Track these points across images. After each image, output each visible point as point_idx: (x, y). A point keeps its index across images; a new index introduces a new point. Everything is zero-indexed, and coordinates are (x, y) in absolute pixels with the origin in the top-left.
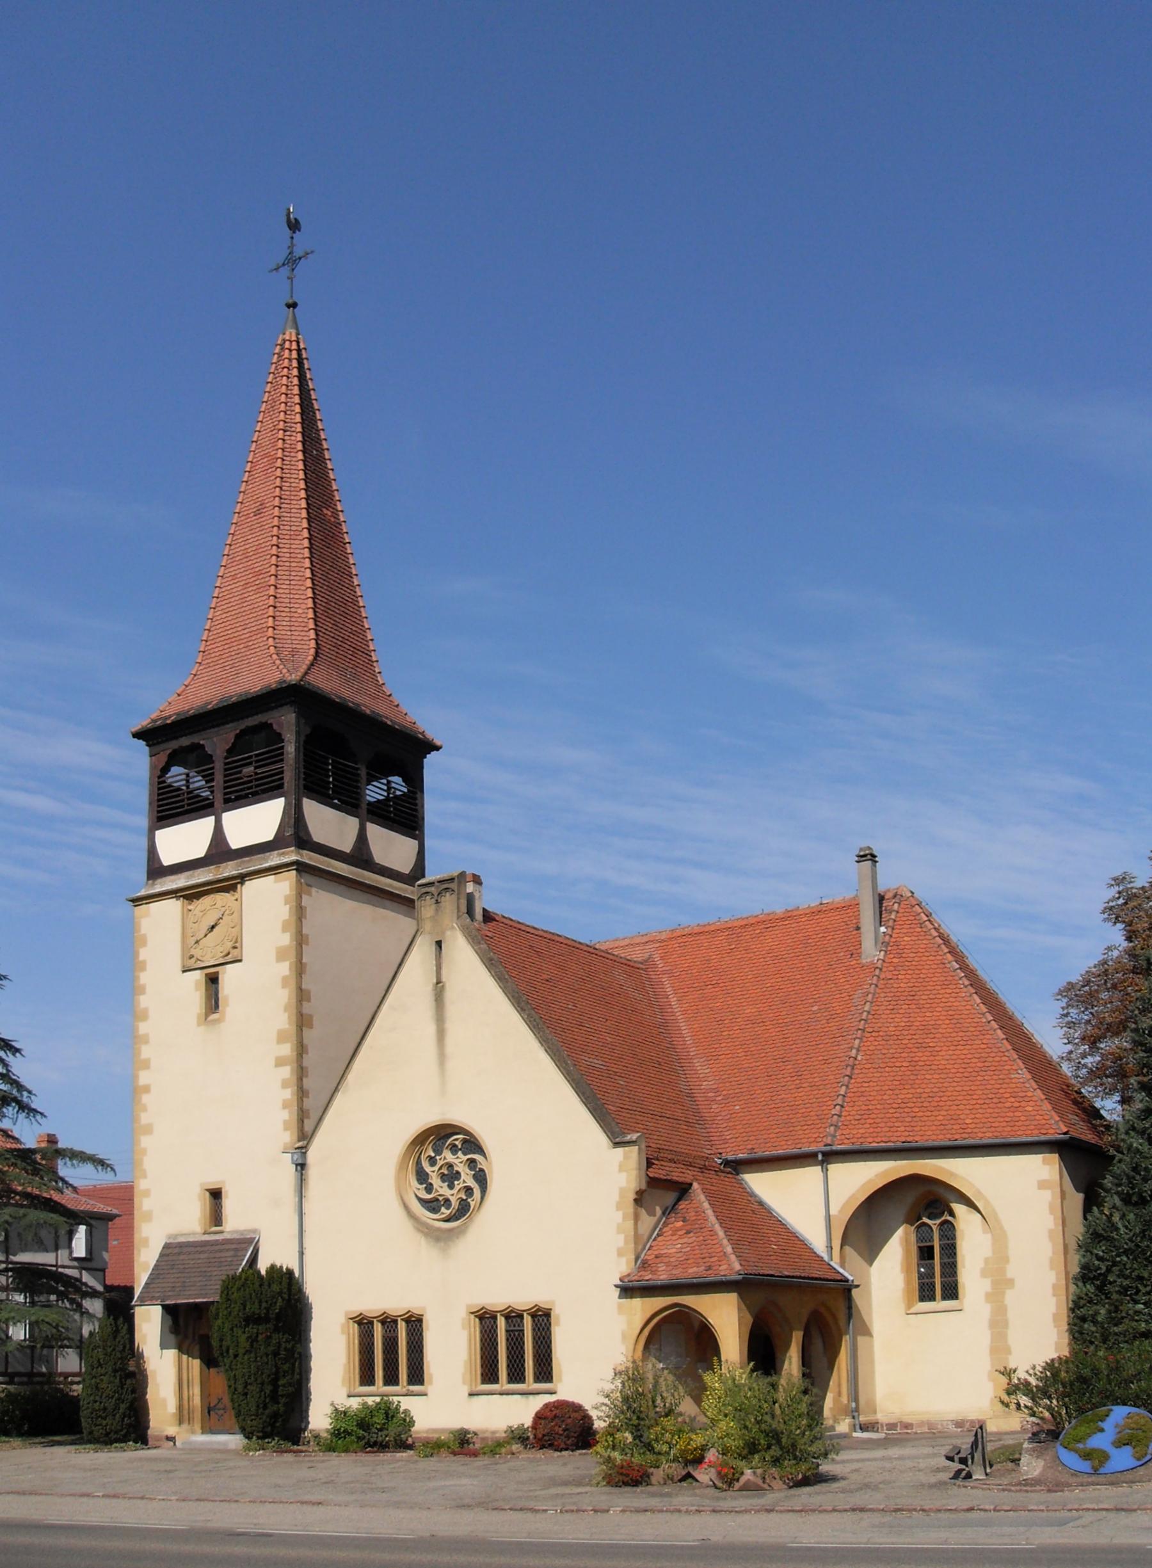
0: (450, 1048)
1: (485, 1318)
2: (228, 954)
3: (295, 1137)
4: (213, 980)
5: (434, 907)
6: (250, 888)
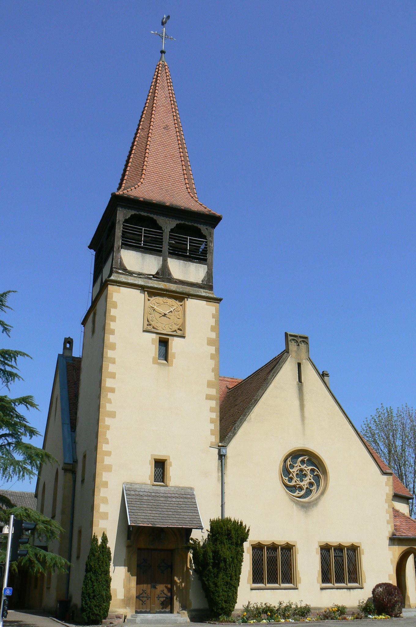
0: (306, 414)
1: (325, 549)
2: (175, 331)
3: (218, 440)
4: (164, 343)
5: (296, 346)
6: (190, 303)
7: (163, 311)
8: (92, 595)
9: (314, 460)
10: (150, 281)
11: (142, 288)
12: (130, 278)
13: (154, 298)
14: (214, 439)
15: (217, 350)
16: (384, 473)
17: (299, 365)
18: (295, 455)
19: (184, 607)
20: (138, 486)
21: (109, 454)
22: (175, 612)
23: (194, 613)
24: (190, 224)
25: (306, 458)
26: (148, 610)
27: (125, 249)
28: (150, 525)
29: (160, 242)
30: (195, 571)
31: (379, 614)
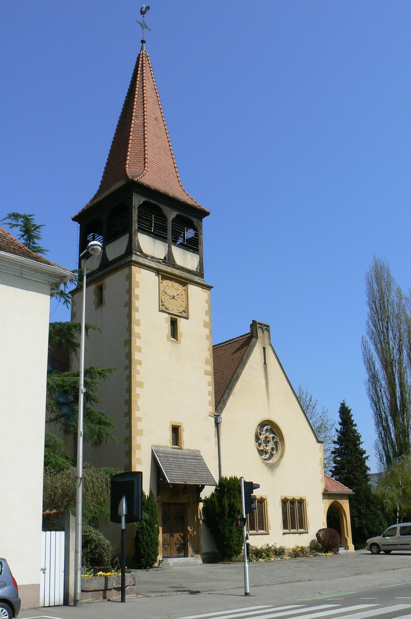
2: (181, 312)
4: (174, 323)
7: (172, 294)
8: (150, 543)
9: (274, 430)
10: (161, 265)
11: (158, 271)
12: (146, 260)
13: (166, 281)
14: (211, 409)
15: (211, 332)
16: (319, 442)
17: (264, 348)
18: (263, 424)
19: (197, 551)
20: (162, 449)
21: (140, 419)
22: (189, 556)
23: (205, 556)
24: (185, 215)
25: (268, 427)
26: (169, 555)
27: (141, 233)
28: (183, 483)
29: (166, 230)
30: (203, 521)
31: (326, 552)
